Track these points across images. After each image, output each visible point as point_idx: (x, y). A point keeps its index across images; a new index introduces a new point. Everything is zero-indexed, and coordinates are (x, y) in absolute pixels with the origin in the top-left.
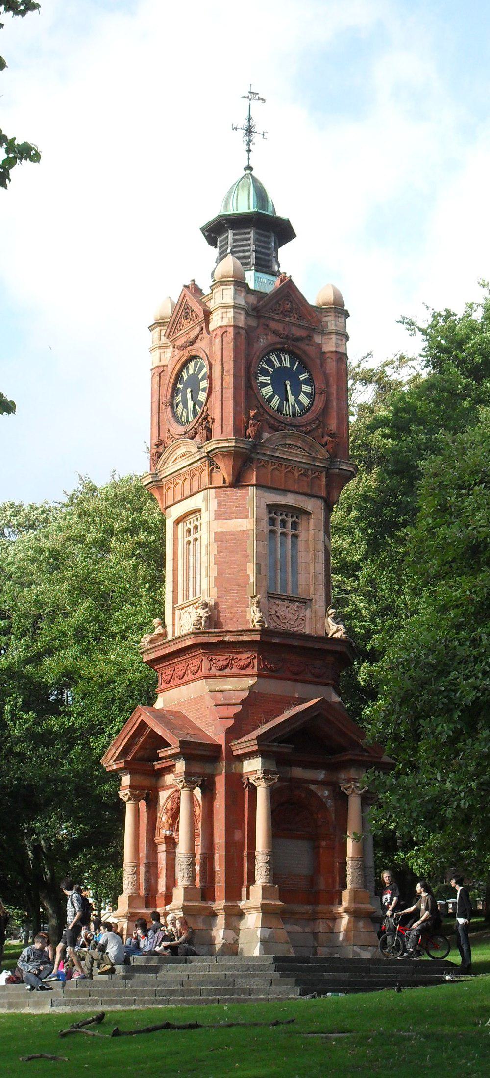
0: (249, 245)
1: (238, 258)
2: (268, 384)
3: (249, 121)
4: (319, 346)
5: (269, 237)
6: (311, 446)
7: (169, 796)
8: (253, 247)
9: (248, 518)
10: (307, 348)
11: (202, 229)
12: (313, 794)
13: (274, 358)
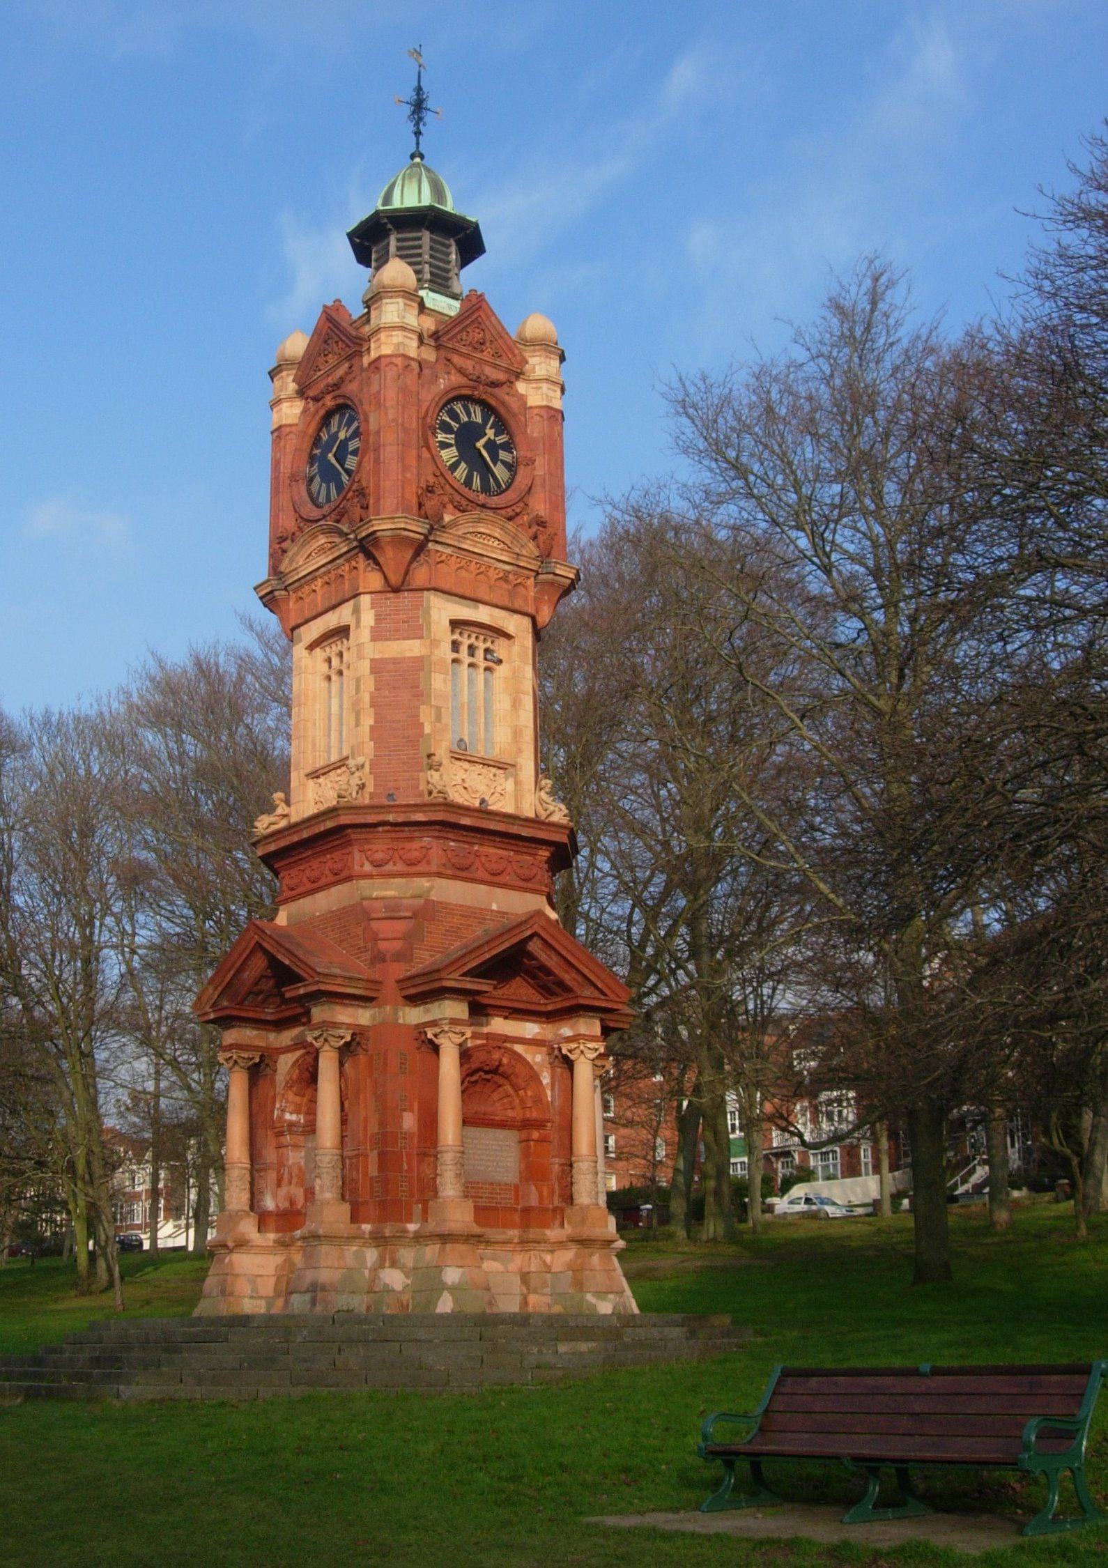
0: (420, 255)
1: (410, 264)
2: (451, 445)
3: (418, 94)
4: (522, 398)
5: (448, 246)
6: (515, 537)
7: (297, 1061)
8: (427, 257)
9: (421, 637)
10: (507, 398)
11: (348, 235)
12: (519, 1057)
13: (458, 407)
